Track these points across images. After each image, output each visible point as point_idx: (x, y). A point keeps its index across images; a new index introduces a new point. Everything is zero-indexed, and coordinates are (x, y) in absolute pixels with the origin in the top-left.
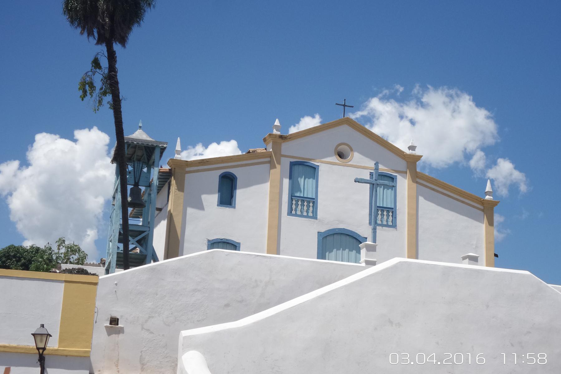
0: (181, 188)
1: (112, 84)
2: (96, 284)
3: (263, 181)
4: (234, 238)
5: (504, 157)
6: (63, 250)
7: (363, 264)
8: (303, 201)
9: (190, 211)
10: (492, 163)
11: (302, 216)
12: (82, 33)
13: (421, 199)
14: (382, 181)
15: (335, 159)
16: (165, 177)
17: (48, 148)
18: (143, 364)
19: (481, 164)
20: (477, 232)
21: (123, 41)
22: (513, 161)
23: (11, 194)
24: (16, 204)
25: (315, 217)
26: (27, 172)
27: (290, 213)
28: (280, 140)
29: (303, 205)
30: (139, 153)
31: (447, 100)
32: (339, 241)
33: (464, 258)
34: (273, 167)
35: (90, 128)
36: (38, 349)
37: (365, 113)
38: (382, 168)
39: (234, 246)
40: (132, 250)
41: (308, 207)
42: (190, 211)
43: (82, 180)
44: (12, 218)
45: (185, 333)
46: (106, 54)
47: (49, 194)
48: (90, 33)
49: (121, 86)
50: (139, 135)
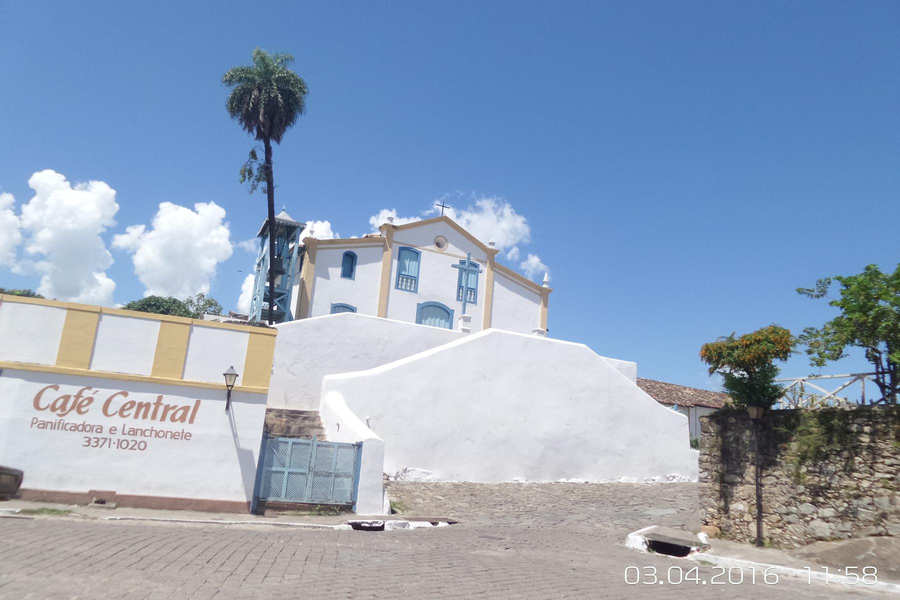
0: (312, 261)
1: (267, 172)
2: (275, 336)
3: (377, 260)
4: (353, 304)
5: (533, 254)
6: (202, 303)
7: (461, 331)
8: (407, 279)
9: (318, 279)
10: (524, 258)
11: (405, 290)
12: (244, 129)
13: (496, 283)
14: (467, 268)
15: (433, 247)
16: (302, 250)
17: (171, 216)
18: (287, 400)
19: (516, 257)
20: (536, 311)
21: (278, 140)
22: (540, 257)
23: (135, 253)
24: (139, 260)
25: (416, 292)
26: (152, 234)
27: (397, 287)
28: (393, 229)
29: (407, 282)
30: (281, 230)
31: (496, 206)
32: (433, 311)
33: (534, 331)
34: (386, 250)
35: (208, 203)
36: (228, 386)
37: (433, 211)
38: (473, 260)
39: (352, 309)
40: (275, 309)
41: (411, 283)
42: (318, 279)
43: (198, 244)
44: (136, 272)
45: (327, 377)
46: (264, 148)
47: (168, 254)
48: (250, 130)
49: (274, 175)
50: (282, 216)
